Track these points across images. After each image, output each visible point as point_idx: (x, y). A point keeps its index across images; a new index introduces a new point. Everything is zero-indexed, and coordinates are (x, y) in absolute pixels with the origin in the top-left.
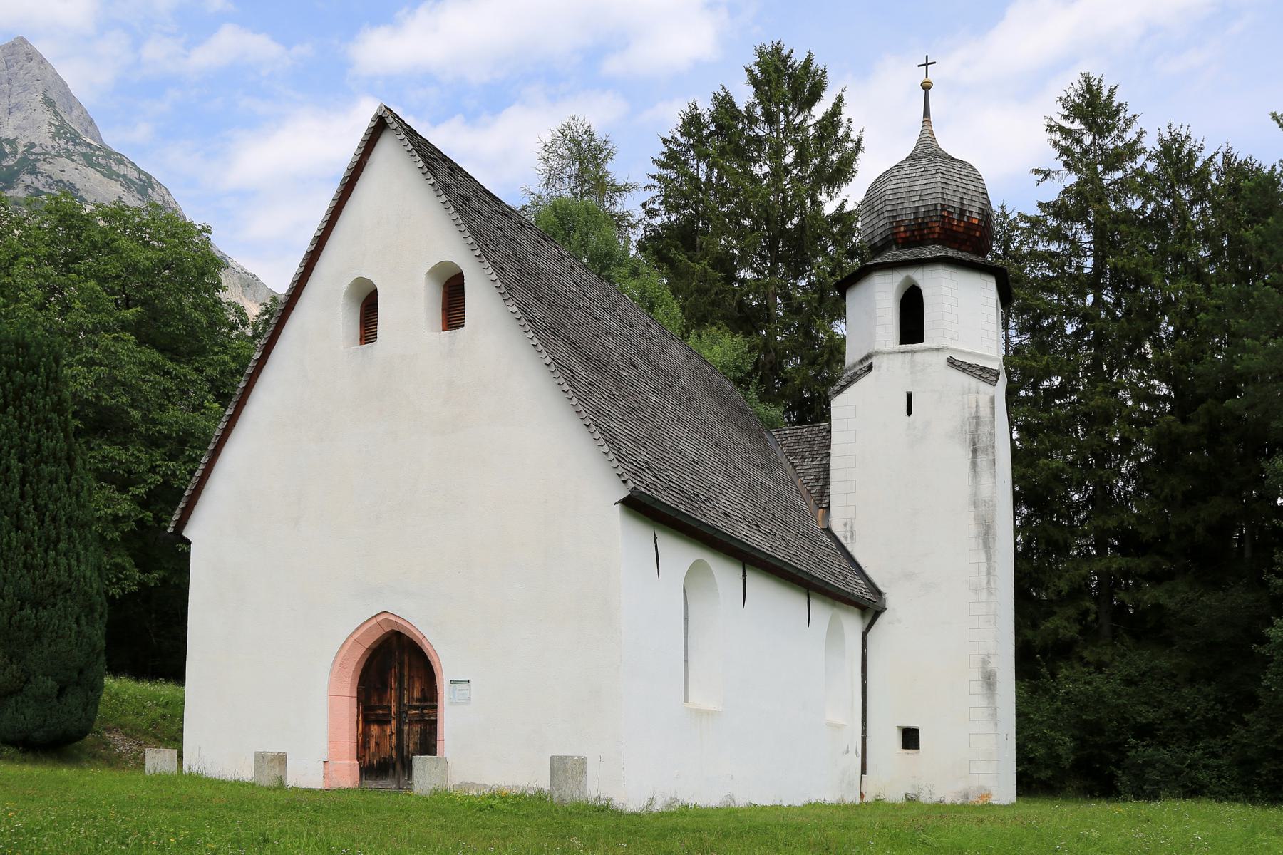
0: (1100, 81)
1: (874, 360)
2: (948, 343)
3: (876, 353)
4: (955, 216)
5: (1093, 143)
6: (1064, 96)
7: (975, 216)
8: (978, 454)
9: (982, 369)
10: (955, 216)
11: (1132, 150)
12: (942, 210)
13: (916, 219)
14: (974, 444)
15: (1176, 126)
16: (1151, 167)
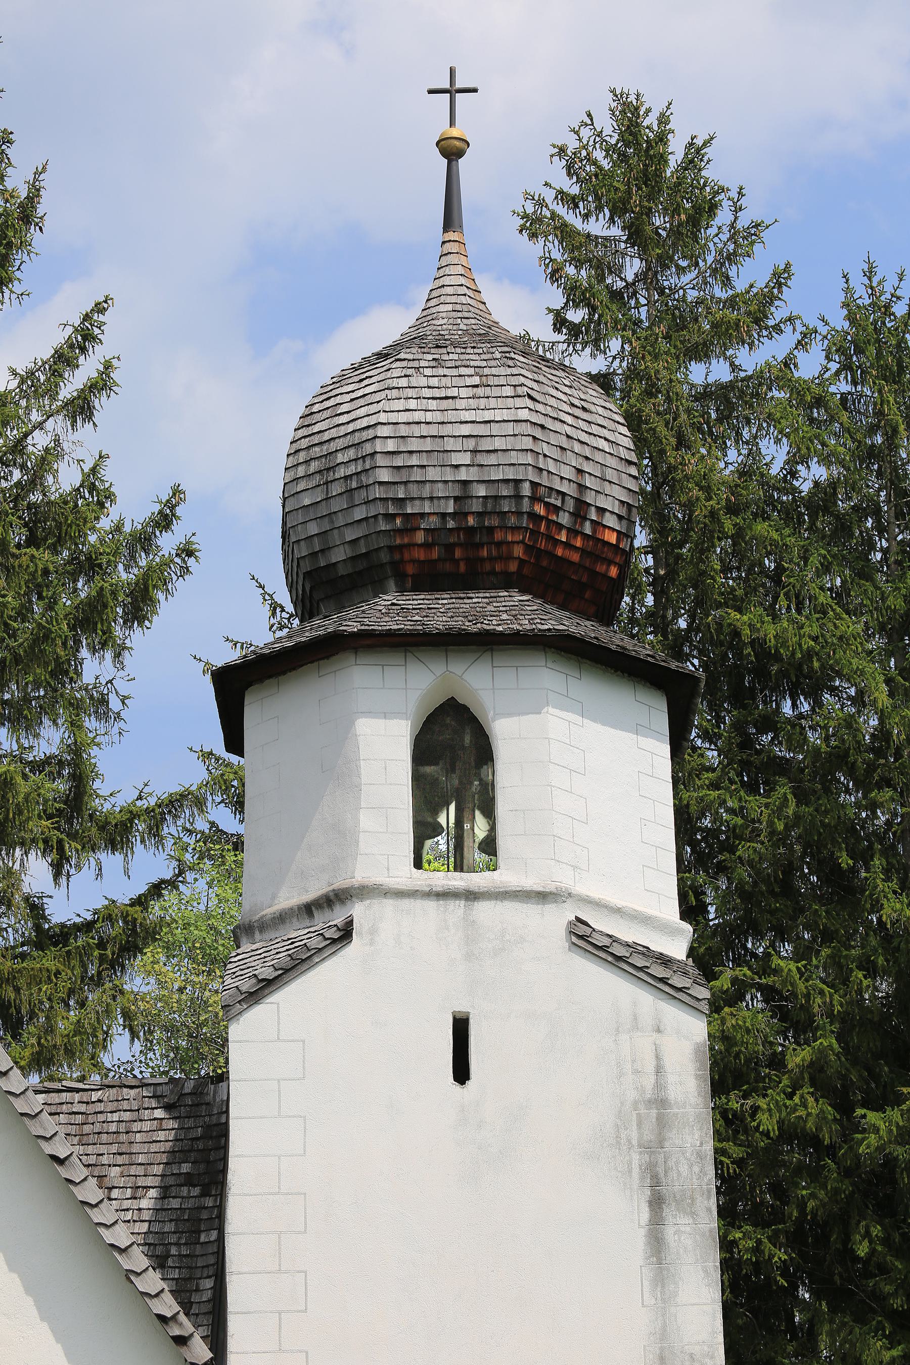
0: (663, 119)
1: (359, 911)
2: (563, 879)
3: (364, 892)
4: (564, 519)
5: (641, 277)
6: (572, 144)
7: (610, 521)
8: (669, 1212)
9: (647, 952)
10: (564, 519)
11: (755, 314)
12: (534, 499)
13: (459, 515)
14: (655, 1183)
15: (886, 272)
16: (810, 365)
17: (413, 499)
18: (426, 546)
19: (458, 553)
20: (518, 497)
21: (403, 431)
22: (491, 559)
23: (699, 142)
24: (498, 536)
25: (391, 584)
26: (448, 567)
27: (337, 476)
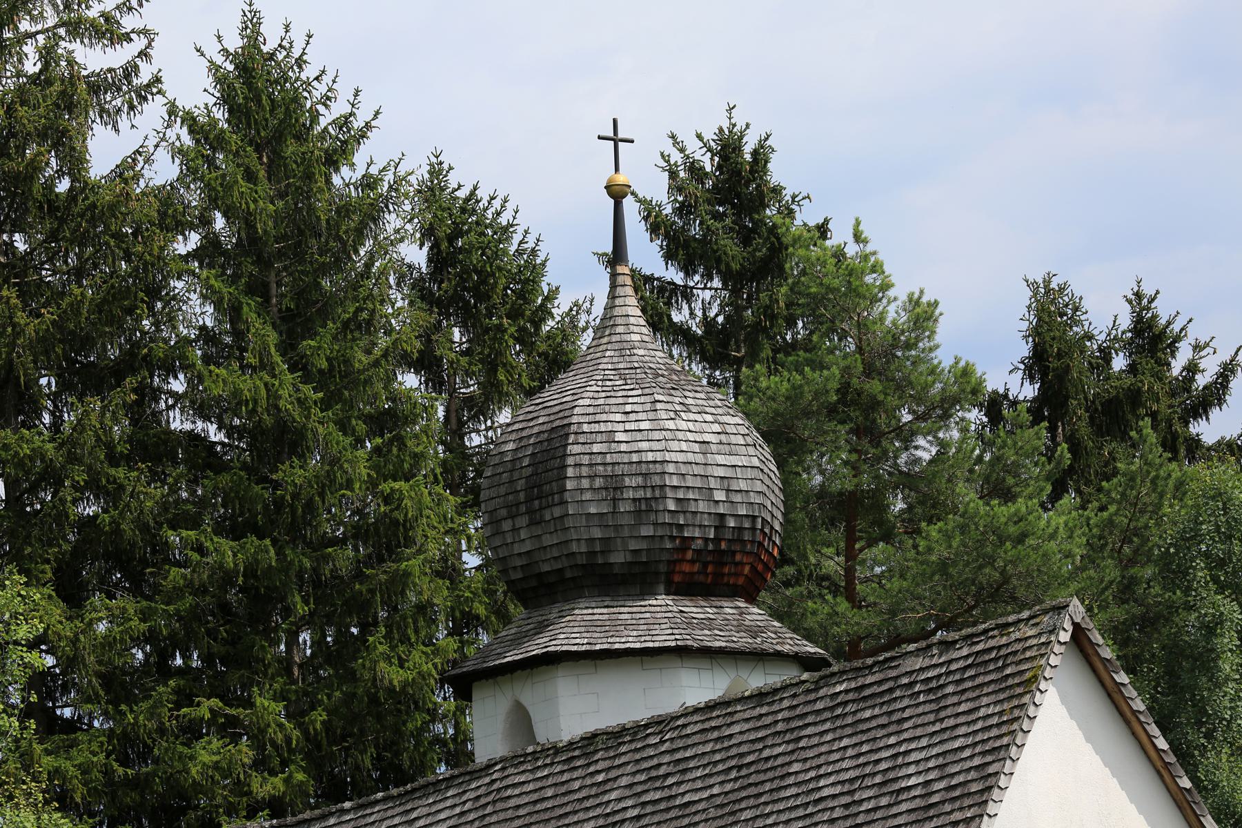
0: (1227, 372)
13: (717, 540)
17: (688, 525)
18: (692, 562)
19: (710, 569)
20: (753, 529)
21: (683, 469)
22: (729, 574)
23: (916, 296)
24: (738, 557)
25: (662, 588)
26: (701, 578)
27: (625, 496)
